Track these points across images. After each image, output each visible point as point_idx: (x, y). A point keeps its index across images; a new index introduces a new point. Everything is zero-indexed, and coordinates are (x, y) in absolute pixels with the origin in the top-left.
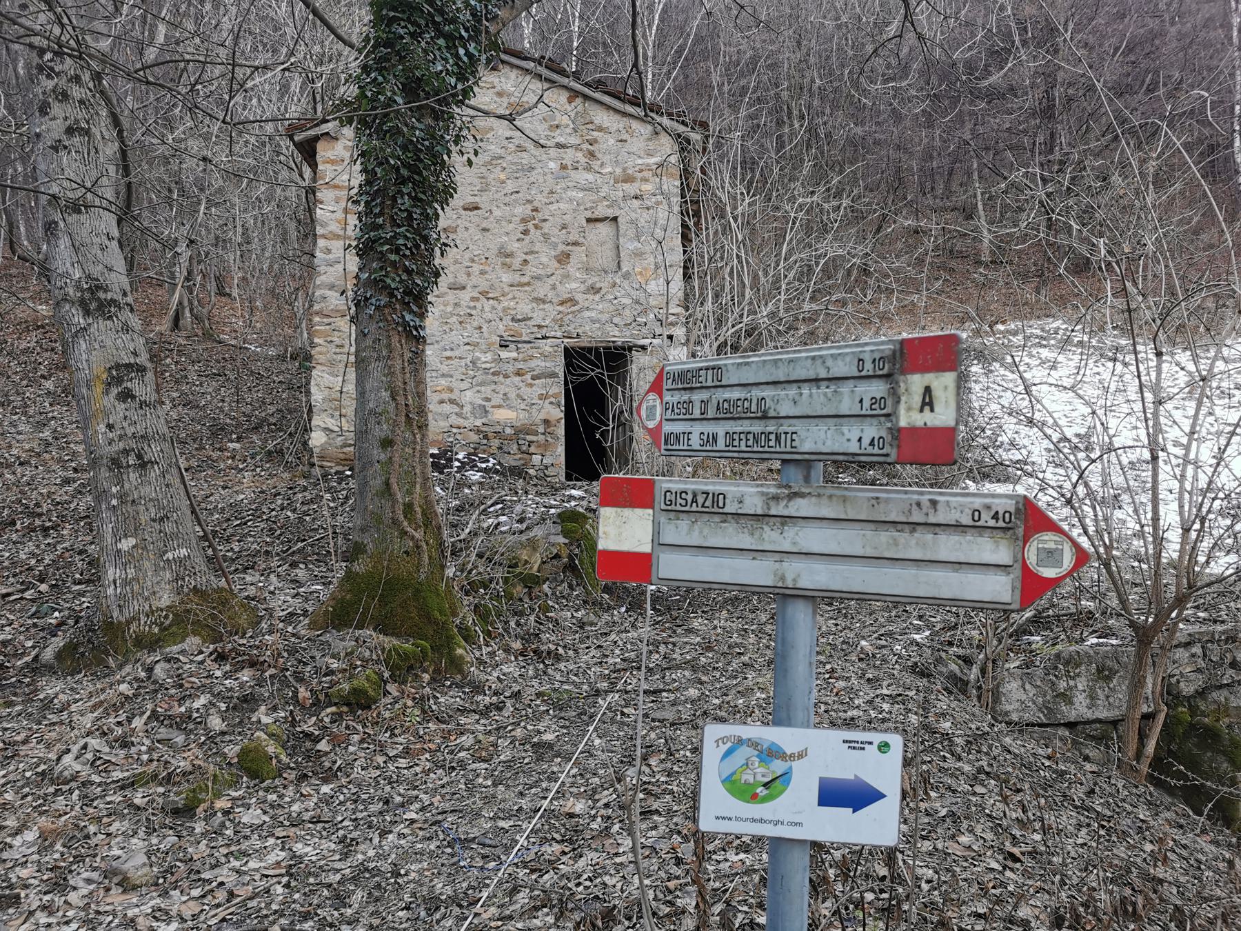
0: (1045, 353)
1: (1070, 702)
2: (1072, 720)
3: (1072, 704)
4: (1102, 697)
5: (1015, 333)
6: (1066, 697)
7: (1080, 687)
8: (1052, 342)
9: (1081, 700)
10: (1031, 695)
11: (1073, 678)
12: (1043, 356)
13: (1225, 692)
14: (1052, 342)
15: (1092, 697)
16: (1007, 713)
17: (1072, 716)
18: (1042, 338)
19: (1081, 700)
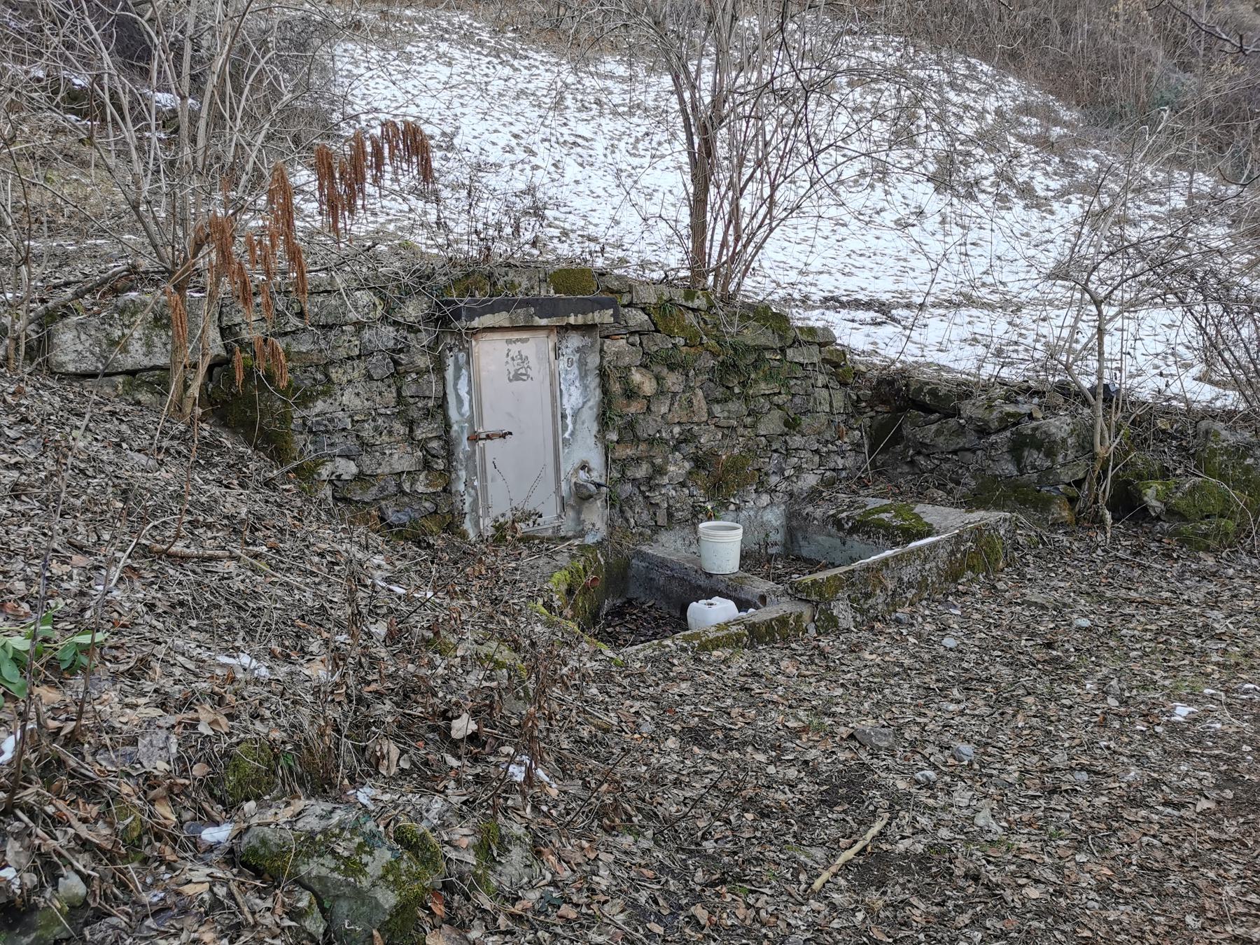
0: (443, 47)
1: (125, 350)
2: (129, 367)
3: (128, 352)
4: (159, 345)
5: (422, 22)
6: (120, 344)
7: (136, 335)
8: (455, 37)
9: (137, 348)
10: (87, 345)
11: (128, 327)
12: (441, 50)
13: (288, 339)
14: (455, 37)
15: (149, 345)
16: (61, 365)
17: (129, 363)
18: (446, 31)
19: (137, 348)
